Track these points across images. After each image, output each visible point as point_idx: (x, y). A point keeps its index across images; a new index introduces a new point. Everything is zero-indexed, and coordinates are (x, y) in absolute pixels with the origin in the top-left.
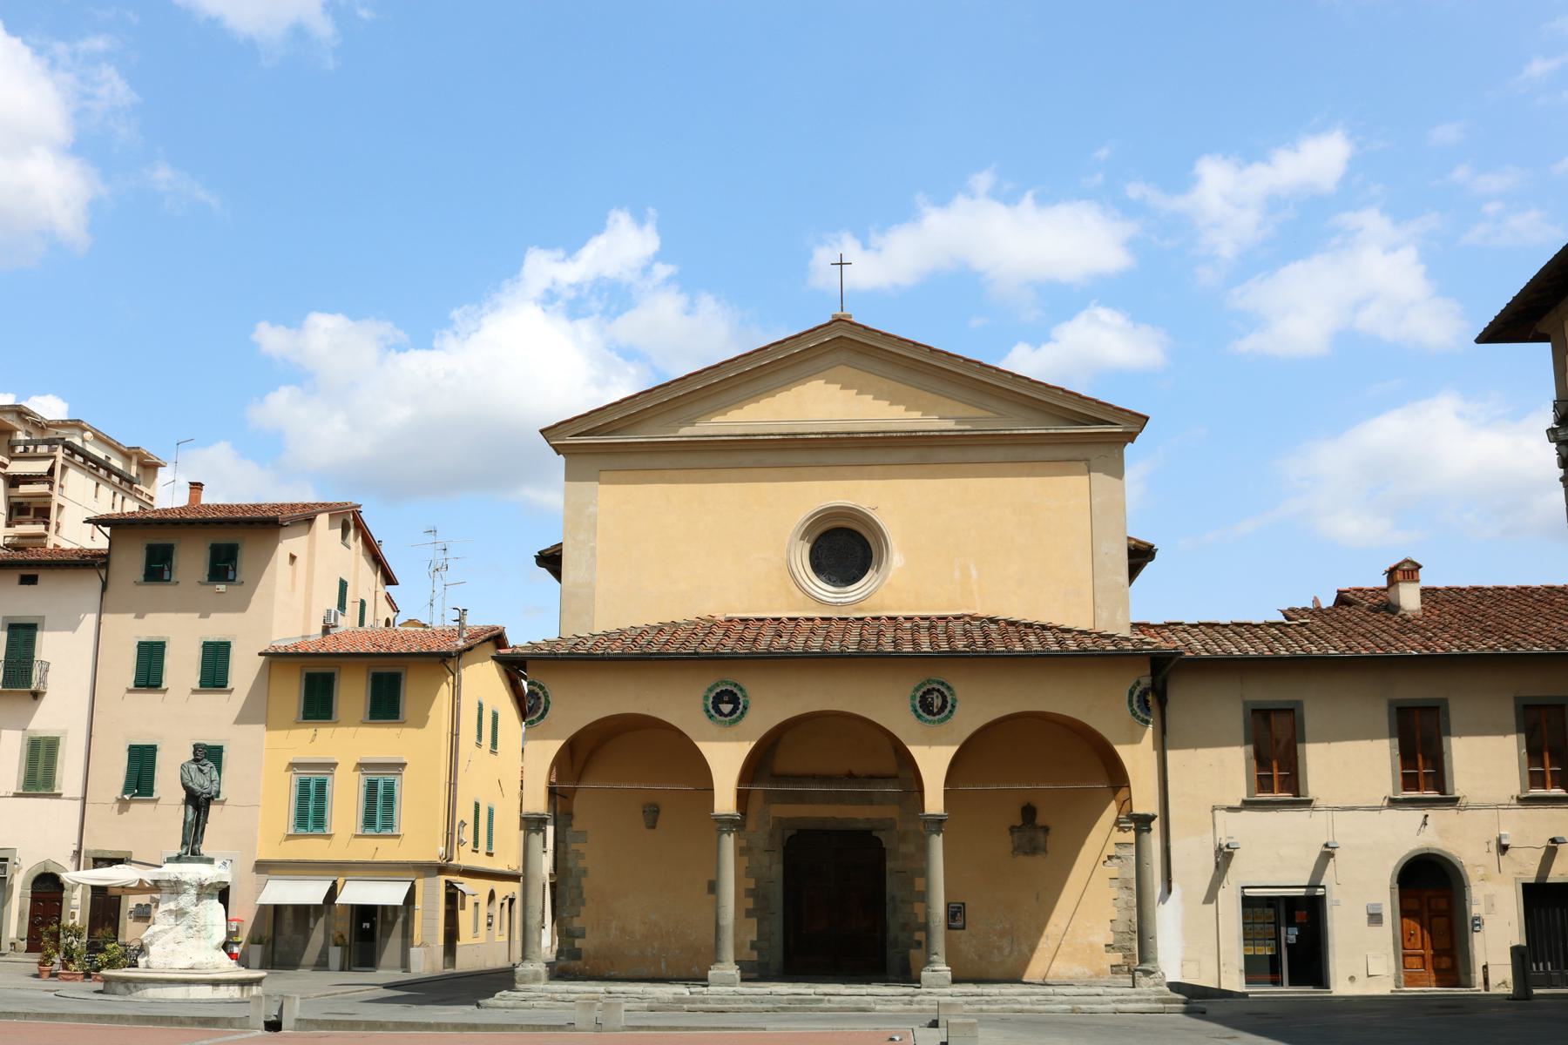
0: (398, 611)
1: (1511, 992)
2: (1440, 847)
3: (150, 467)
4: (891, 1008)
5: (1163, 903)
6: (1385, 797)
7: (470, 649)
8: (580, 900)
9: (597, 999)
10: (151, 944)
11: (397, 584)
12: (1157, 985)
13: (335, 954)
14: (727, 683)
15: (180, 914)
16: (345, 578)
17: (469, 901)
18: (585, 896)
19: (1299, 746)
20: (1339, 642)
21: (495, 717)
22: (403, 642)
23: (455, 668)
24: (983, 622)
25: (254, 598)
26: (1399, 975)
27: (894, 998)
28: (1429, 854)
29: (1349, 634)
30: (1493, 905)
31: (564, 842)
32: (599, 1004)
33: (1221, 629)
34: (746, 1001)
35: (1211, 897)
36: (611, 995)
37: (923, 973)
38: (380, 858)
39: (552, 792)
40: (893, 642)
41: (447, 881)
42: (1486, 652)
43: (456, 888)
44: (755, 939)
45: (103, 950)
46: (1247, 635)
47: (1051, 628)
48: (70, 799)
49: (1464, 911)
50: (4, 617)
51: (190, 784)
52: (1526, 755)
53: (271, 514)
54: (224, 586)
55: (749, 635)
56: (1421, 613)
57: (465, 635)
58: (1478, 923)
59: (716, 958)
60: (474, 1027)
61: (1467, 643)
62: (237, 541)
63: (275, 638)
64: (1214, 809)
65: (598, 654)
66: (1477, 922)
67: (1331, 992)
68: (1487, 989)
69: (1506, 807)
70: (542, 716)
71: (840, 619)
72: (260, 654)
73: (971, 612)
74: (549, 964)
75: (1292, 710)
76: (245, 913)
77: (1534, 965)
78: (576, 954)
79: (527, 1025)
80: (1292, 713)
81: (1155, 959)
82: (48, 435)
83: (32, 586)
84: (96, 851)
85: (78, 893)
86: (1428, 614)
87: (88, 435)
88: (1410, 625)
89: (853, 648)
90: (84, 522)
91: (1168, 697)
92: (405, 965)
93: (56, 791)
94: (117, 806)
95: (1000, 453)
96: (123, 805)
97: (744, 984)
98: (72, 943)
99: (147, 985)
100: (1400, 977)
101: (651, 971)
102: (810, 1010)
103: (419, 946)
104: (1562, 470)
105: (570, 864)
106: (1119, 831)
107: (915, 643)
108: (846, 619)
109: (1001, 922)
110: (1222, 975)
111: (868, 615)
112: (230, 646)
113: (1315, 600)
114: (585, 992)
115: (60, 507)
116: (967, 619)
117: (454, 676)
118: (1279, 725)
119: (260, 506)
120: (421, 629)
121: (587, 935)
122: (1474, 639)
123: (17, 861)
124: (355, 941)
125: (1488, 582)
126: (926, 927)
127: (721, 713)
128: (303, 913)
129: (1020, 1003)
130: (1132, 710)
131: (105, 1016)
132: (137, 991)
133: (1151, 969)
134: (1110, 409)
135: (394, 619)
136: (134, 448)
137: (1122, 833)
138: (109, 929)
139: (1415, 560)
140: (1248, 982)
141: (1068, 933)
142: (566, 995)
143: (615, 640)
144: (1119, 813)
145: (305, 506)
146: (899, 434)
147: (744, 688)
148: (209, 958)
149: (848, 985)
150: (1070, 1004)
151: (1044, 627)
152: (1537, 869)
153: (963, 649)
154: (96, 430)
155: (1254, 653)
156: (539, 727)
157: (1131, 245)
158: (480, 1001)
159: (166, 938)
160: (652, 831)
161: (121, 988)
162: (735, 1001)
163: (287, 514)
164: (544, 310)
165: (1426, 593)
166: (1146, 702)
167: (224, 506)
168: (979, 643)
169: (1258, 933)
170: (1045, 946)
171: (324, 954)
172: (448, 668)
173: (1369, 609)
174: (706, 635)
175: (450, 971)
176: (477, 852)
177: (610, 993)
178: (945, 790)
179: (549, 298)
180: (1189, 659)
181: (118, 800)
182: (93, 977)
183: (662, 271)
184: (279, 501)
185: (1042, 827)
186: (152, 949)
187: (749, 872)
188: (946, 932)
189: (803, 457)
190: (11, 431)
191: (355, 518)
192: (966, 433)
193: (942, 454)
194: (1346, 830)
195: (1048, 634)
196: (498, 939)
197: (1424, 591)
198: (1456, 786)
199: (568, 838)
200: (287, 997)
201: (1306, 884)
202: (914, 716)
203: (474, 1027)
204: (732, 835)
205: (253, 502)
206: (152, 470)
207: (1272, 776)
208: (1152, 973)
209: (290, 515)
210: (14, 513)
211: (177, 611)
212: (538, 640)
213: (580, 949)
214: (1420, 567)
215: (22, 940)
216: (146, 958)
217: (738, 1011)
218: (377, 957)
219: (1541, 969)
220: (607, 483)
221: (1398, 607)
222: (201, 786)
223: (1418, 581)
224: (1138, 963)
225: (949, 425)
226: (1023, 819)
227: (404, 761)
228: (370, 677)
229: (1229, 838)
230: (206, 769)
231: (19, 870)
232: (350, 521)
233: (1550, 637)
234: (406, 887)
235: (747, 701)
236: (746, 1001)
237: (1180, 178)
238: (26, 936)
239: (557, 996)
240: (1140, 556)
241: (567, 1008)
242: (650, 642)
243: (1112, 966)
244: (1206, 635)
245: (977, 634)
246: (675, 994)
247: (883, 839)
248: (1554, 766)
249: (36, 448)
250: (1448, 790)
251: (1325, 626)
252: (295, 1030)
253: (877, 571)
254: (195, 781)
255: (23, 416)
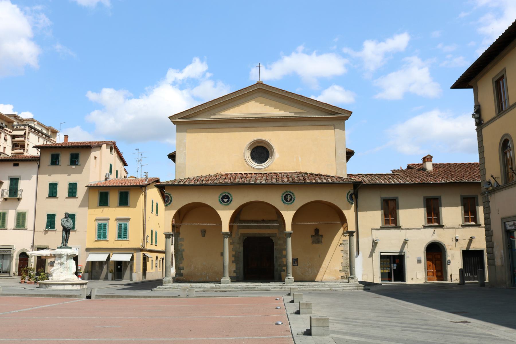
0: (128, 174)
1: (459, 282)
2: (438, 240)
3: (54, 132)
4: (276, 289)
5: (357, 258)
6: (422, 225)
7: (149, 184)
8: (182, 258)
9: (187, 288)
10: (53, 273)
11: (127, 166)
12: (355, 282)
13: (110, 275)
14: (226, 193)
15: (61, 264)
16: (111, 164)
17: (150, 260)
18: (184, 257)
19: (397, 210)
20: (409, 179)
21: (157, 205)
22: (129, 183)
23: (144, 190)
24: (303, 174)
25: (84, 170)
26: (426, 278)
27: (277, 287)
28: (435, 242)
29: (412, 177)
30: (453, 257)
31: (177, 241)
32: (188, 290)
33: (374, 176)
34: (232, 288)
35: (371, 255)
36: (192, 287)
37: (285, 279)
38: (123, 247)
39: (173, 226)
40: (276, 180)
41: (143, 254)
42: (452, 182)
43: (146, 255)
44: (235, 269)
45: (40, 275)
46: (382, 177)
47: (323, 175)
48: (30, 230)
49: (445, 259)
50: (9, 176)
51: (64, 225)
52: (464, 213)
53: (89, 144)
54: (75, 166)
55: (232, 178)
56: (433, 171)
57: (148, 180)
58: (449, 262)
59: (223, 275)
60: (150, 297)
61: (447, 179)
62: (78, 153)
63: (90, 182)
64: (372, 229)
65: (186, 184)
66: (449, 262)
67: (406, 283)
68: (451, 281)
69: (457, 228)
70: (170, 203)
71: (260, 173)
72: (86, 186)
73: (299, 171)
74: (173, 278)
75: (395, 200)
76: (82, 264)
77: (465, 274)
78: (181, 275)
79: (166, 296)
80: (395, 201)
81: (355, 274)
82: (24, 123)
83: (17, 167)
84: (38, 246)
85: (33, 258)
86: (435, 171)
87: (36, 123)
88: (429, 174)
89: (264, 182)
90: (32, 147)
91: (358, 196)
92: (131, 279)
93: (26, 228)
94: (44, 232)
95: (307, 123)
96: (46, 232)
97: (232, 283)
98: (31, 273)
99: (52, 285)
100: (426, 278)
101: (204, 279)
102: (252, 290)
103: (135, 273)
104: (476, 127)
105: (179, 248)
106: (343, 236)
107: (282, 180)
108: (262, 173)
109: (309, 264)
110: (374, 278)
111: (268, 172)
112: (77, 184)
113: (401, 168)
114: (184, 286)
115: (28, 145)
116: (298, 173)
117: (144, 192)
118: (391, 204)
119: (85, 142)
120: (134, 179)
121: (184, 269)
122: (449, 178)
123: (14, 249)
124: (116, 271)
125: (452, 162)
126: (286, 265)
127: (224, 202)
128: (101, 263)
129: (314, 288)
130: (348, 200)
131: (38, 295)
132: (49, 287)
133: (353, 277)
134: (341, 109)
135: (127, 176)
136: (49, 127)
137: (344, 237)
138: (42, 269)
139: (431, 155)
140: (382, 280)
141: (329, 267)
142: (178, 287)
143: (192, 180)
144: (344, 231)
145: (99, 142)
146: (277, 118)
147: (231, 194)
148: (71, 277)
149: (263, 283)
150: (329, 288)
151: (321, 175)
152: (466, 246)
153: (297, 182)
154: (38, 121)
155: (384, 183)
156: (169, 206)
157: (346, 66)
158: (152, 289)
159: (57, 271)
160: (203, 238)
161: (44, 286)
162: (229, 288)
163: (93, 144)
164: (173, 87)
165: (434, 165)
166: (352, 197)
167: (75, 143)
168: (302, 180)
169: (385, 266)
170: (322, 271)
171: (107, 276)
172: (142, 190)
173: (417, 170)
174: (219, 178)
175: (145, 280)
176: (152, 245)
177: (191, 286)
178: (292, 224)
179: (174, 84)
180: (365, 185)
181: (44, 230)
182: (37, 283)
183: (208, 75)
184: (91, 141)
185: (321, 235)
186: (53, 274)
187: (233, 250)
188: (292, 267)
189: (248, 125)
190: (13, 122)
191: (114, 146)
192: (298, 117)
193: (290, 123)
194: (411, 235)
195: (322, 177)
196: (159, 270)
197: (433, 165)
198: (443, 222)
199: (178, 240)
200: (93, 288)
201: (399, 251)
202: (282, 202)
203: (150, 297)
204: (228, 238)
205: (83, 141)
206: (55, 133)
207: (389, 220)
208: (354, 278)
209: (94, 144)
210: (14, 146)
211: (61, 174)
212: (168, 180)
213: (182, 273)
214: (432, 157)
215: (17, 272)
216: (51, 277)
217: (230, 291)
218: (123, 276)
219: (467, 275)
220: (189, 133)
221: (426, 169)
222: (67, 226)
223: (432, 161)
224: (349, 275)
225: (292, 114)
226: (315, 233)
227: (130, 218)
228: (119, 193)
229: (376, 238)
230: (69, 220)
231: (15, 251)
232: (113, 147)
233: (471, 178)
234: (131, 255)
235: (232, 198)
236: (232, 288)
237: (359, 46)
238: (18, 271)
239: (175, 287)
240: (350, 154)
241: (178, 291)
242: (202, 181)
243: (341, 276)
244: (369, 178)
245: (301, 177)
246: (211, 286)
247: (273, 239)
248: (472, 216)
249: (20, 127)
250: (441, 223)
251: (405, 175)
252: (95, 298)
253: (271, 159)
254: (65, 224)
255: (16, 117)
